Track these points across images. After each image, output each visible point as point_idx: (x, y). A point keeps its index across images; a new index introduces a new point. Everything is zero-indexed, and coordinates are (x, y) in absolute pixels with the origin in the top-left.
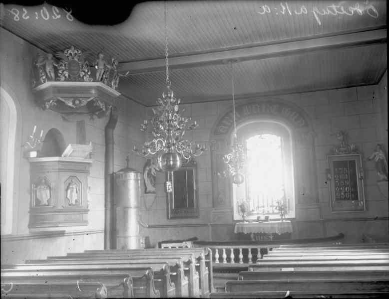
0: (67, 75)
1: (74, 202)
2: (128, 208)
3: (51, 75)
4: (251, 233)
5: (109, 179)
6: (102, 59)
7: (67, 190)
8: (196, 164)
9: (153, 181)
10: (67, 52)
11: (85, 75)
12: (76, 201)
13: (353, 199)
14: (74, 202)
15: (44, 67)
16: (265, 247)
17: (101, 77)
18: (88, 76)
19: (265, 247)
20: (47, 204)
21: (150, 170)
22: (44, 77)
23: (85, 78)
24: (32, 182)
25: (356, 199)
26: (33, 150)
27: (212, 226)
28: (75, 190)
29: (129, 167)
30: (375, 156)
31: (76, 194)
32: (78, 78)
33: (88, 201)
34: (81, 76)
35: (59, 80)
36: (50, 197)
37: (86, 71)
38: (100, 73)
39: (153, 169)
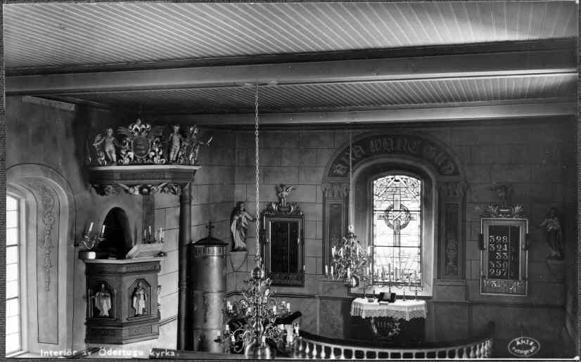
0: (132, 156)
1: (141, 313)
2: (208, 292)
3: (111, 156)
4: (370, 318)
5: (185, 249)
6: (177, 133)
7: (132, 298)
8: (303, 215)
9: (244, 234)
10: (132, 127)
11: (155, 156)
12: (144, 310)
13: (511, 278)
14: (141, 313)
15: (103, 147)
16: (385, 351)
17: (175, 156)
18: (158, 157)
19: (385, 351)
20: (108, 315)
21: (240, 220)
22: (103, 159)
23: (155, 159)
24: (88, 286)
25: (493, 353)
26: (91, 250)
27: (321, 298)
28: (142, 297)
29: (215, 236)
30: (547, 224)
31: (144, 301)
32: (147, 160)
33: (159, 305)
34: (151, 157)
35: (121, 164)
36: (112, 306)
37: (157, 150)
38: (175, 152)
39: (243, 217)
